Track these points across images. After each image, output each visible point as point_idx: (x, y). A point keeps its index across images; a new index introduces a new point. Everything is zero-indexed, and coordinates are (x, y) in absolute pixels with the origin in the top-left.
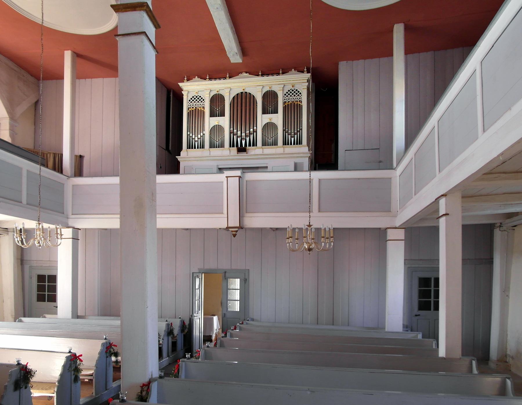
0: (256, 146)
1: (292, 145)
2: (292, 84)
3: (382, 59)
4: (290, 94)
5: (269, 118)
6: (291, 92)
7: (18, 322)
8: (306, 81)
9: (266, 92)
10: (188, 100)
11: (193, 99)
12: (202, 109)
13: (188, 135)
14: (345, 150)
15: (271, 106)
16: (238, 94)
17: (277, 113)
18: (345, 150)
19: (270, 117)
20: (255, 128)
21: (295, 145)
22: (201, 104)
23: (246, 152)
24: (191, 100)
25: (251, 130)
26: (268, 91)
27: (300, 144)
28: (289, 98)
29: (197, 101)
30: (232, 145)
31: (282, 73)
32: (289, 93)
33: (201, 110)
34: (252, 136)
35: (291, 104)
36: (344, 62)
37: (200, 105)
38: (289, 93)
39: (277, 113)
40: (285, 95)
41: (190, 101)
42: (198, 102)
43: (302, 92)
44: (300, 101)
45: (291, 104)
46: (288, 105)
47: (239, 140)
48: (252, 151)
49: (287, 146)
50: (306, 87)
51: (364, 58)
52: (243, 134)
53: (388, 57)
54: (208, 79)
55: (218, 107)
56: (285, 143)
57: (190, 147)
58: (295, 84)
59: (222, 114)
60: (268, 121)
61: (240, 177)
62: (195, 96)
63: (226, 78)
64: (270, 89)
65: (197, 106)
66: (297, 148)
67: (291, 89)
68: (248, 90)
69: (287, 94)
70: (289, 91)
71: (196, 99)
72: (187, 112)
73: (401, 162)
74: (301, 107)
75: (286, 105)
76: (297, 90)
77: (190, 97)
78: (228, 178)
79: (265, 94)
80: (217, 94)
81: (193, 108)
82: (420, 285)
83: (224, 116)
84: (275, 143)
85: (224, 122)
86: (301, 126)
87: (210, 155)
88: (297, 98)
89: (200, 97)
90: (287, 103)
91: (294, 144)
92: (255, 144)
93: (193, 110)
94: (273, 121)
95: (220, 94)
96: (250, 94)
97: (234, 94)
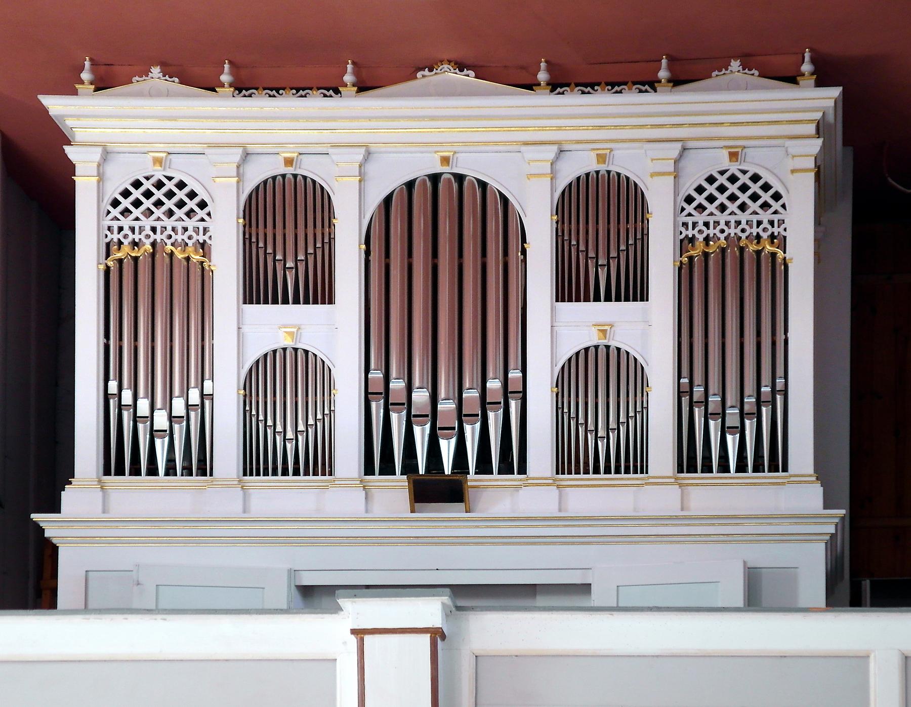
4: (705, 190)
8: (811, 129)
9: (578, 179)
10: (108, 199)
11: (137, 194)
12: (196, 258)
16: (410, 185)
23: (461, 506)
24: (126, 203)
26: (588, 175)
27: (774, 468)
32: (711, 189)
33: (188, 259)
35: (723, 250)
40: (689, 200)
44: (772, 237)
47: (421, 434)
49: (699, 475)
52: (446, 406)
60: (591, 338)
61: (436, 635)
64: (603, 168)
67: (722, 173)
70: (137, 184)
71: (159, 194)
75: (691, 258)
77: (694, 177)
80: (284, 176)
91: (741, 467)
93: (136, 259)
96: (483, 185)
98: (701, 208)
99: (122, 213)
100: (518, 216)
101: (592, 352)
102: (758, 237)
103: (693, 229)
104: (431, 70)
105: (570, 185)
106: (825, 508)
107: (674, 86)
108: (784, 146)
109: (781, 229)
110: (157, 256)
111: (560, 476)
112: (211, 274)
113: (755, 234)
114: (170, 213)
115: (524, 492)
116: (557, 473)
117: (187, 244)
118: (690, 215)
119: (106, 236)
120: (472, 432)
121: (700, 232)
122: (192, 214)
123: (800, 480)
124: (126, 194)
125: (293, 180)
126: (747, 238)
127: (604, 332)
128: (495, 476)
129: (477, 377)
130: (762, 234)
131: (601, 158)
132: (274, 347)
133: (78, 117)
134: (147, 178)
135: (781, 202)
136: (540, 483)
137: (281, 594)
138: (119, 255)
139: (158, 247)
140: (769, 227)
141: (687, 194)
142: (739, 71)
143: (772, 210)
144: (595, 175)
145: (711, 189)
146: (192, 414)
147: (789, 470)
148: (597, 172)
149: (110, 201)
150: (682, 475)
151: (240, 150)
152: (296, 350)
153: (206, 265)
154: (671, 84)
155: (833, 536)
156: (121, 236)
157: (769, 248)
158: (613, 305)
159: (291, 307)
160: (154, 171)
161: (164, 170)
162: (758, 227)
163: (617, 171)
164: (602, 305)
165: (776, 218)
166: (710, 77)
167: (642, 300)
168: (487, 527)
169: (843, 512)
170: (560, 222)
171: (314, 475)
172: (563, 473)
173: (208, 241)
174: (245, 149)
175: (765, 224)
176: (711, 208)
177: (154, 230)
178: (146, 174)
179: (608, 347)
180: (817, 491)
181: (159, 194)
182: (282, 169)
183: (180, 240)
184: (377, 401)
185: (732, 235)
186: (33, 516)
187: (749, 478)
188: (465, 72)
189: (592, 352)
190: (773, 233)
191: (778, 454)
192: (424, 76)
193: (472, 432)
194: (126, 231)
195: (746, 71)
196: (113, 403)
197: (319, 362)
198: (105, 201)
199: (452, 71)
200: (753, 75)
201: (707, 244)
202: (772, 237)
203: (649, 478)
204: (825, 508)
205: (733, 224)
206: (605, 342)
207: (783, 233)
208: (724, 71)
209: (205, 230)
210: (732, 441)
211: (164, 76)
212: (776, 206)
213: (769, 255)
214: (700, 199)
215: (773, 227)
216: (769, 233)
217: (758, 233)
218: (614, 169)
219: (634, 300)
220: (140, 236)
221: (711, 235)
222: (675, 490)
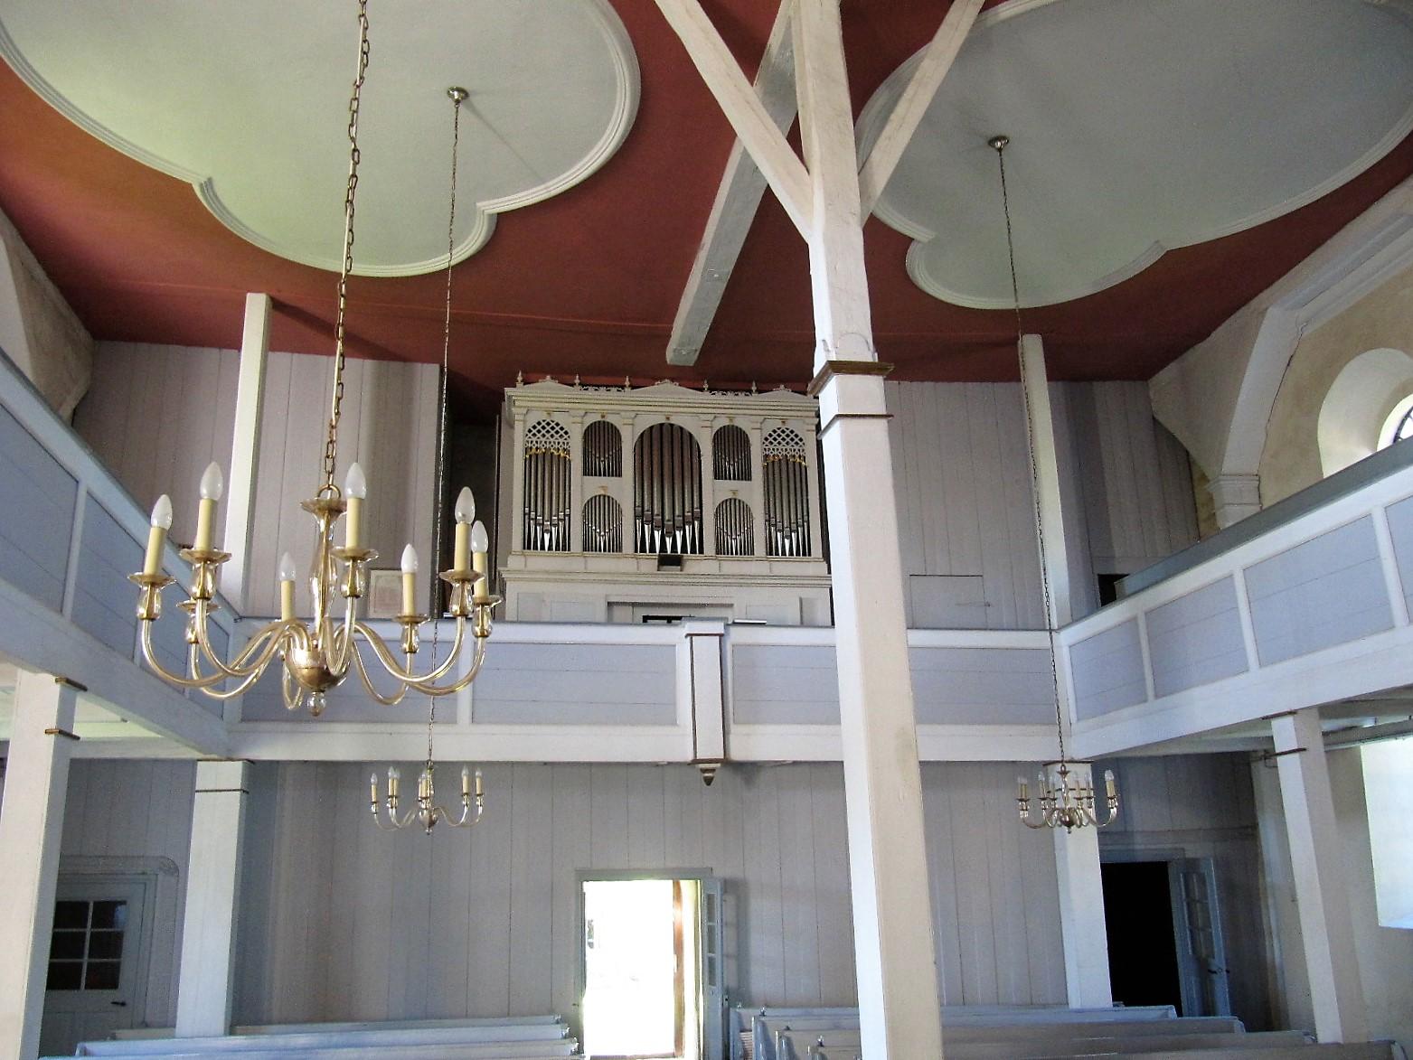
1: (537, 549)
3: (970, 385)
6: (544, 428)
7: (80, 1055)
8: (517, 403)
11: (539, 427)
13: (525, 514)
15: (604, 457)
16: (652, 428)
17: (620, 475)
19: (734, 488)
21: (695, 553)
27: (564, 549)
28: (775, 448)
31: (580, 384)
32: (775, 435)
33: (560, 455)
35: (544, 453)
38: (775, 435)
39: (620, 475)
45: (780, 460)
48: (694, 565)
51: (293, 351)
53: (994, 382)
54: (580, 384)
55: (602, 454)
57: (529, 544)
61: (721, 636)
63: (623, 389)
66: (780, 563)
67: (544, 421)
68: (675, 420)
69: (771, 439)
75: (530, 456)
76: (792, 432)
77: (532, 421)
78: (694, 638)
82: (116, 968)
83: (620, 475)
84: (747, 549)
85: (622, 489)
87: (586, 568)
89: (557, 424)
90: (534, 450)
92: (698, 547)
93: (537, 455)
96: (681, 429)
98: (534, 435)
120: (679, 535)
127: (734, 493)
131: (603, 417)
137: (601, 613)
152: (604, 496)
176: (539, 435)
181: (548, 428)
182: (599, 419)
196: (527, 517)
209: (568, 443)
212: (566, 436)
218: (736, 425)
222: (523, 559)
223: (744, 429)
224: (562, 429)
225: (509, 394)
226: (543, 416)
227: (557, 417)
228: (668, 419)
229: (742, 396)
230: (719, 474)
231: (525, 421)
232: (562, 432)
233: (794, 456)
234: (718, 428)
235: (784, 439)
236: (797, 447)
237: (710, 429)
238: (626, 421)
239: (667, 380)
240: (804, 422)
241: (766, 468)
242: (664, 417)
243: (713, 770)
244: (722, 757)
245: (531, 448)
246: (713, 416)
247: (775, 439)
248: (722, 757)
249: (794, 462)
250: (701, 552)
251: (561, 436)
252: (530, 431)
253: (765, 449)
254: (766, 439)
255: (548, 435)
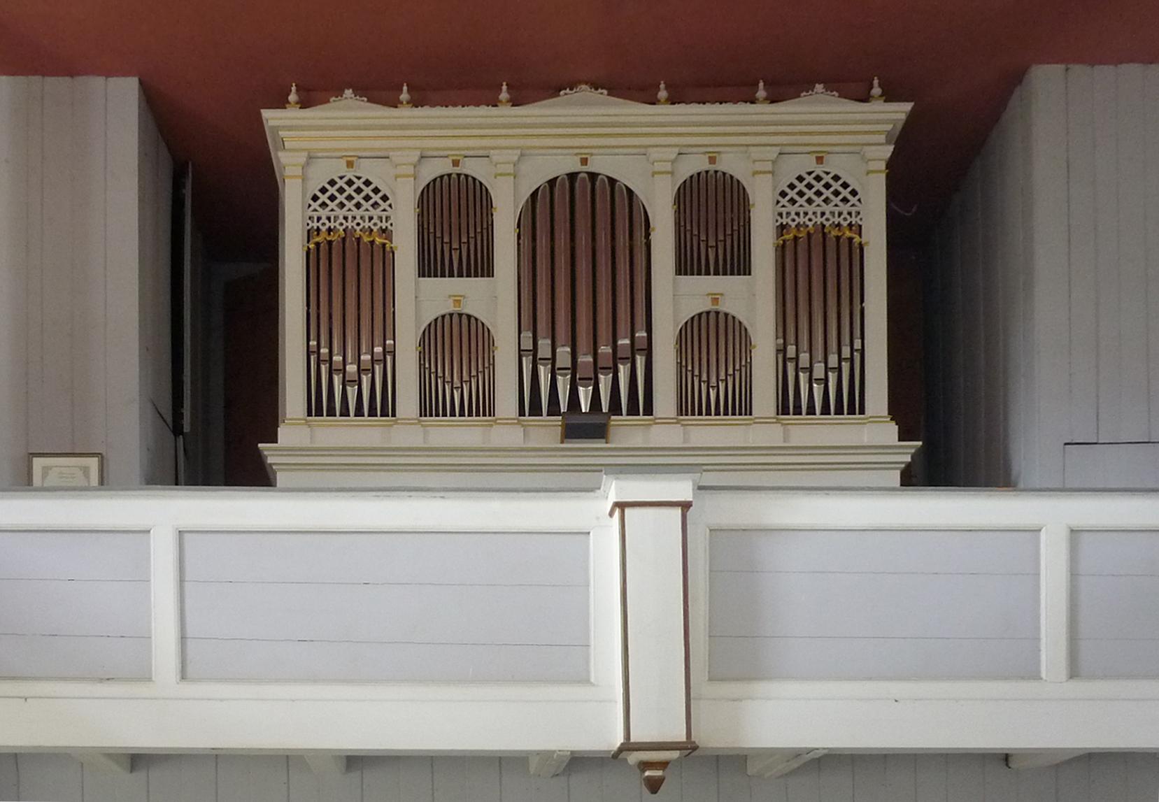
0: (394, 415)
2: (711, 149)
5: (708, 295)
8: (882, 138)
9: (691, 177)
10: (310, 195)
11: (332, 190)
12: (378, 241)
14: (1066, 444)
16: (552, 182)
18: (1066, 444)
20: (641, 334)
22: (354, 218)
23: (604, 440)
24: (323, 198)
25: (624, 342)
26: (699, 174)
27: (852, 411)
29: (354, 202)
30: (531, 406)
32: (801, 186)
33: (372, 242)
34: (380, 368)
36: (1059, 66)
37: (802, 214)
40: (783, 194)
41: (315, 198)
42: (358, 206)
43: (393, 193)
44: (850, 225)
45: (809, 234)
46: (796, 238)
49: (791, 416)
50: (884, 167)
52: (585, 359)
55: (711, 231)
56: (787, 405)
58: (593, 151)
59: (482, 266)
60: (704, 305)
62: (341, 178)
64: (712, 168)
65: (354, 224)
67: (810, 173)
68: (603, 165)
70: (332, 183)
72: (306, 249)
73: (462, 494)
74: (856, 253)
75: (318, 244)
76: (836, 178)
77: (318, 179)
79: (682, 190)
80: (449, 175)
81: (330, 230)
83: (750, 274)
86: (857, 332)
88: (840, 214)
89: (367, 183)
91: (826, 410)
92: (642, 404)
93: (330, 243)
94: (727, 306)
95: (467, 176)
96: (612, 181)
97: (535, 178)
98: (324, 205)
99: (373, 206)
100: (642, 207)
101: (447, 319)
102: (318, 230)
103: (335, 222)
104: (571, 89)
105: (685, 182)
106: (899, 440)
107: (513, 106)
108: (645, 154)
109: (858, 219)
110: (348, 240)
111: (423, 418)
112: (391, 255)
113: (315, 228)
114: (342, 205)
115: (655, 429)
116: (421, 416)
117: (372, 230)
118: (315, 210)
119: (308, 224)
120: (605, 381)
121: (845, 219)
122: (376, 206)
123: (876, 420)
124: (323, 190)
125: (714, 175)
126: (361, 230)
128: (624, 417)
129: (734, 339)
130: (321, 227)
131: (456, 163)
132: (443, 312)
133: (290, 128)
134: (359, 178)
135: (857, 197)
136: (666, 422)
138: (317, 239)
139: (348, 232)
140: (327, 222)
141: (781, 190)
142: (822, 93)
143: (329, 208)
144: (705, 175)
145: (801, 186)
146: (377, 367)
147: (866, 413)
148: (707, 172)
149: (311, 197)
150: (681, 417)
151: (306, 154)
152: (460, 315)
153: (388, 248)
154: (299, 106)
155: (909, 465)
156: (371, 224)
157: (848, 234)
158: (720, 278)
159: (455, 280)
160: (346, 172)
161: (355, 171)
162: (370, 221)
163: (610, 175)
164: (712, 279)
165: (853, 210)
166: (799, 96)
167: (489, 276)
168: (428, 456)
169: (920, 443)
170: (678, 212)
171: (699, 415)
172: (426, 416)
173: (389, 227)
174: (309, 153)
175: (845, 215)
176: (332, 205)
177: (346, 218)
178: (340, 175)
179: (717, 313)
180: (893, 429)
183: (367, 227)
184: (527, 356)
185: (350, 227)
186: (260, 445)
187: (543, 421)
188: (600, 91)
189: (447, 319)
190: (330, 227)
191: (388, 405)
192: (566, 94)
193: (605, 381)
194: (324, 220)
195: (358, 97)
196: (422, 367)
197: (737, 323)
198: (308, 196)
199: (589, 89)
200: (834, 95)
201: (798, 230)
202: (850, 225)
203: (656, 419)
204: (899, 440)
205: (802, 214)
206: (715, 307)
207: (860, 223)
208: (810, 92)
209: (387, 218)
210: (818, 389)
211: (355, 96)
213: (381, 246)
214: (792, 194)
215: (330, 222)
216: (327, 227)
217: (318, 227)
219: (467, 276)
220: (335, 224)
221: (802, 223)
223: (737, 176)
224: (376, 191)
225: (271, 123)
226: (336, 169)
227: (367, 170)
228: (584, 162)
229: (483, 110)
230: (687, 264)
231: (304, 179)
232: (376, 198)
233: (839, 225)
234: (686, 176)
235: (819, 193)
236: (845, 208)
237: (770, 176)
238: (501, 168)
239: (584, 87)
240: (863, 157)
241: (781, 250)
242: (706, 158)
243: (663, 765)
244: (684, 739)
245: (318, 230)
246: (777, 149)
247: (801, 194)
248: (684, 739)
249: (372, 242)
250: (649, 410)
251: (375, 205)
252: (315, 198)
253: (781, 215)
254: (783, 194)
255: (349, 205)
